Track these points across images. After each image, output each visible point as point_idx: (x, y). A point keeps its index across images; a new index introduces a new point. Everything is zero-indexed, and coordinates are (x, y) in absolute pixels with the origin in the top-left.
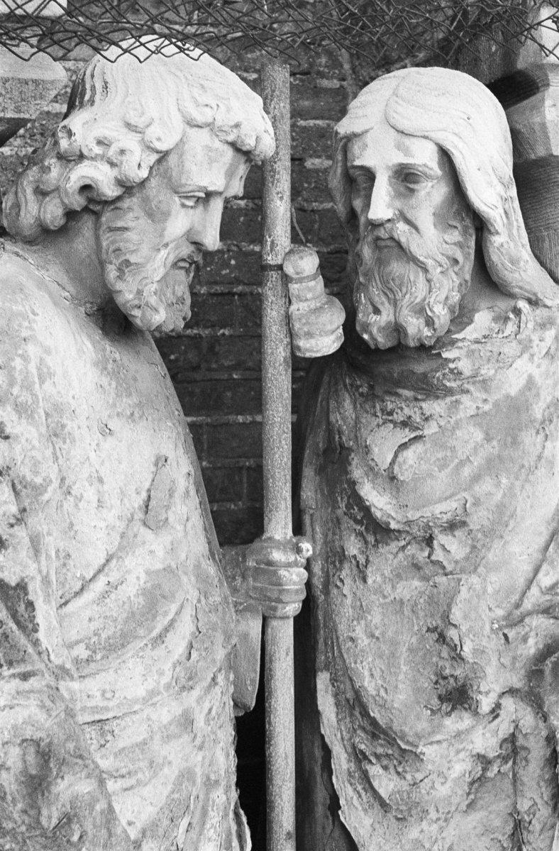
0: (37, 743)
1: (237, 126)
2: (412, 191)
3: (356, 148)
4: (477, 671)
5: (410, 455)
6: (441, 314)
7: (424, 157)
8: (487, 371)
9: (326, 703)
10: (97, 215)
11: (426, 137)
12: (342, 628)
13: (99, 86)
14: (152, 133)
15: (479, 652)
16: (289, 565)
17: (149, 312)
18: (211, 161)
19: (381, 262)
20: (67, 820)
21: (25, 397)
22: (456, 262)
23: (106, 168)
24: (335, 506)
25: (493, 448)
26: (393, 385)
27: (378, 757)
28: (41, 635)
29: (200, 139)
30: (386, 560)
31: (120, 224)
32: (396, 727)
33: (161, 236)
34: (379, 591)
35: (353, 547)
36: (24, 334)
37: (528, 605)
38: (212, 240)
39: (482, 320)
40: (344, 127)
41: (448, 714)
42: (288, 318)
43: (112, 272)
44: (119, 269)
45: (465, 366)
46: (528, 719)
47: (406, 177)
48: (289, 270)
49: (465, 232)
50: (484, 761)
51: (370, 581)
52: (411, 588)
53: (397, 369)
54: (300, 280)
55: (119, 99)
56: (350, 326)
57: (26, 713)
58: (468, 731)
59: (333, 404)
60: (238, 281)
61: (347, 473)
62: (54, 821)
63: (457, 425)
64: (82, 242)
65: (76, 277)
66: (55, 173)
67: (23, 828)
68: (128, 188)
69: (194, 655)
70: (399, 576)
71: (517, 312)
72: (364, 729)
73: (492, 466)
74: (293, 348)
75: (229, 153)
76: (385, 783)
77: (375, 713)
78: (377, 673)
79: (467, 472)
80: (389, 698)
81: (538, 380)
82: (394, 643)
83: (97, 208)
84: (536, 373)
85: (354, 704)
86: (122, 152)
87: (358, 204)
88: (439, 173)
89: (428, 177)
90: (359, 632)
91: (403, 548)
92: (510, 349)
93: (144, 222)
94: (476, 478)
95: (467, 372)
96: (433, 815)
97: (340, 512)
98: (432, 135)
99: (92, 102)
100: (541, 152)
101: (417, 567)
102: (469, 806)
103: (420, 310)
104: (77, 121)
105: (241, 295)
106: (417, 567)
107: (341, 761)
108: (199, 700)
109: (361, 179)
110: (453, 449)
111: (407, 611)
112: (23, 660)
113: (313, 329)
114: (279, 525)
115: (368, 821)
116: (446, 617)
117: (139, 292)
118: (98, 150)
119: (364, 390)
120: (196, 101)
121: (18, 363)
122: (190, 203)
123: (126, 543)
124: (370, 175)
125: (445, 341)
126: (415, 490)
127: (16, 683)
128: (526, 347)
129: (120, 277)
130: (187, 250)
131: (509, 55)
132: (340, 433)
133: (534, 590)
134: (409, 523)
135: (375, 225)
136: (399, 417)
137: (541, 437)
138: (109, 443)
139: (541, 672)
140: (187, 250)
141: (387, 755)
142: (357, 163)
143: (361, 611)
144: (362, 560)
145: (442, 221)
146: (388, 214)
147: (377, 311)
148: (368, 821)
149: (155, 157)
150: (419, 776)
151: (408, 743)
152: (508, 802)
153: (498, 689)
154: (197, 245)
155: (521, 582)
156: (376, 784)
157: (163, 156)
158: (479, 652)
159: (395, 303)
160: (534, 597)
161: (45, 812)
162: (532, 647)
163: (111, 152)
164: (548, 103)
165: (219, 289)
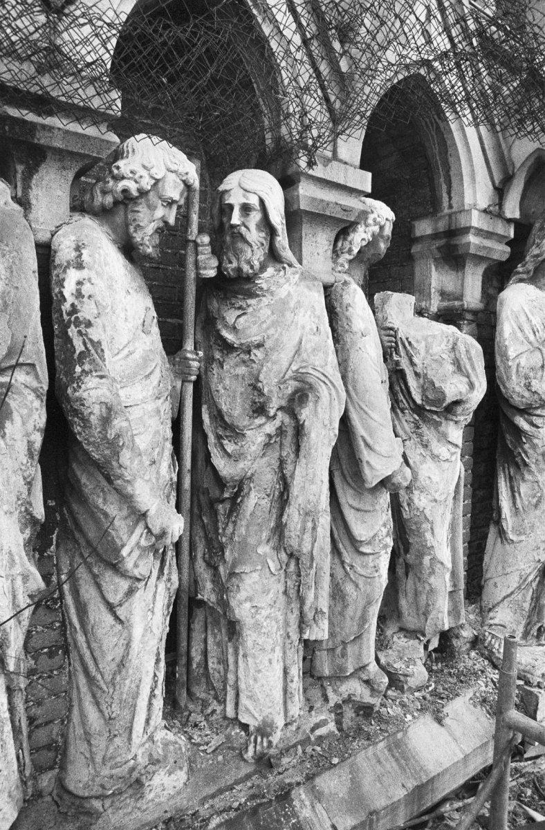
0: (106, 404)
1: (187, 174)
2: (248, 215)
3: (226, 197)
4: (269, 399)
5: (242, 320)
6: (257, 264)
7: (254, 201)
8: (273, 288)
9: (206, 417)
10: (126, 205)
11: (255, 193)
12: (213, 387)
13: (130, 150)
14: (153, 171)
15: (271, 391)
16: (193, 360)
17: (146, 248)
18: (175, 187)
19: (233, 243)
20: (118, 436)
21: (99, 269)
22: (263, 244)
23: (133, 183)
24: (209, 341)
25: (274, 317)
26: (235, 294)
27: (227, 437)
28: (107, 363)
29: (172, 177)
30: (231, 361)
31: (136, 209)
32: (235, 424)
33: (153, 216)
34: (228, 371)
35: (218, 355)
36: (99, 245)
37: (287, 377)
38: (172, 221)
39: (270, 271)
40: (222, 188)
41: (256, 418)
42: (196, 262)
43: (132, 229)
44: (135, 228)
45: (265, 286)
46: (287, 420)
47: (246, 209)
48: (199, 241)
49: (266, 234)
50: (270, 436)
51: (225, 368)
52: (242, 370)
53: (236, 288)
54: (203, 245)
55: (140, 156)
56: (219, 268)
57: (102, 391)
58: (263, 424)
59: (208, 301)
60: (161, 263)
61: (215, 327)
62: (113, 436)
63: (261, 308)
64: (119, 219)
65: (114, 230)
66: (111, 183)
67: (99, 440)
68: (143, 193)
69: (161, 385)
70: (237, 366)
71: (284, 268)
72: (221, 426)
73: (275, 324)
74: (198, 274)
75: (182, 185)
76: (230, 447)
77: (226, 419)
78: (228, 403)
79: (264, 326)
80: (232, 412)
81: (292, 293)
82: (235, 392)
83: (127, 202)
84: (292, 291)
85: (218, 416)
86: (141, 177)
87: (225, 219)
88: (259, 208)
89: (255, 209)
90: (220, 387)
91: (238, 355)
92: (282, 281)
93: (146, 209)
94: (268, 328)
95: (265, 288)
96: (249, 458)
97: (211, 343)
98: (258, 192)
99: (127, 157)
100: (295, 207)
101: (244, 362)
102: (263, 454)
103: (249, 262)
104: (121, 163)
105: (163, 269)
106: (244, 362)
107: (212, 439)
108: (162, 404)
109: (227, 210)
110: (259, 317)
111: (240, 379)
112: (101, 370)
113: (207, 266)
114: (189, 345)
115: (223, 462)
116: (258, 380)
117: (143, 239)
118: (131, 175)
119: (222, 296)
120: (172, 162)
121: (97, 255)
122: (165, 204)
123: (135, 338)
124: (231, 207)
125: (256, 275)
126: (243, 332)
127: (98, 379)
128: (288, 280)
129: (135, 231)
130: (161, 224)
131: (284, 169)
132: (212, 312)
133: (290, 372)
134: (242, 344)
135: (233, 227)
136: (237, 306)
137: (293, 314)
138: (129, 297)
139: (294, 399)
140: (161, 224)
141: (231, 436)
142: (227, 202)
143: (221, 380)
144: (221, 359)
145: (258, 227)
146: (238, 222)
147: (231, 262)
148: (223, 462)
149: (153, 181)
150: (243, 443)
151: (240, 430)
152: (278, 454)
153: (277, 406)
154: (166, 223)
155: (284, 370)
156: (226, 447)
157: (157, 181)
158: (271, 391)
159: (238, 259)
160: (290, 373)
161: (109, 432)
162: (290, 391)
163: (136, 177)
164: (300, 187)
165: (154, 265)
